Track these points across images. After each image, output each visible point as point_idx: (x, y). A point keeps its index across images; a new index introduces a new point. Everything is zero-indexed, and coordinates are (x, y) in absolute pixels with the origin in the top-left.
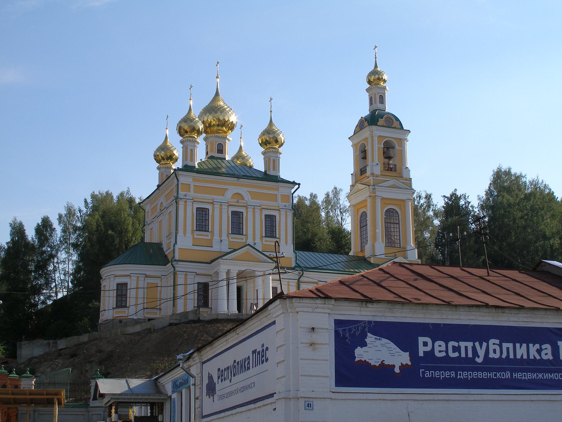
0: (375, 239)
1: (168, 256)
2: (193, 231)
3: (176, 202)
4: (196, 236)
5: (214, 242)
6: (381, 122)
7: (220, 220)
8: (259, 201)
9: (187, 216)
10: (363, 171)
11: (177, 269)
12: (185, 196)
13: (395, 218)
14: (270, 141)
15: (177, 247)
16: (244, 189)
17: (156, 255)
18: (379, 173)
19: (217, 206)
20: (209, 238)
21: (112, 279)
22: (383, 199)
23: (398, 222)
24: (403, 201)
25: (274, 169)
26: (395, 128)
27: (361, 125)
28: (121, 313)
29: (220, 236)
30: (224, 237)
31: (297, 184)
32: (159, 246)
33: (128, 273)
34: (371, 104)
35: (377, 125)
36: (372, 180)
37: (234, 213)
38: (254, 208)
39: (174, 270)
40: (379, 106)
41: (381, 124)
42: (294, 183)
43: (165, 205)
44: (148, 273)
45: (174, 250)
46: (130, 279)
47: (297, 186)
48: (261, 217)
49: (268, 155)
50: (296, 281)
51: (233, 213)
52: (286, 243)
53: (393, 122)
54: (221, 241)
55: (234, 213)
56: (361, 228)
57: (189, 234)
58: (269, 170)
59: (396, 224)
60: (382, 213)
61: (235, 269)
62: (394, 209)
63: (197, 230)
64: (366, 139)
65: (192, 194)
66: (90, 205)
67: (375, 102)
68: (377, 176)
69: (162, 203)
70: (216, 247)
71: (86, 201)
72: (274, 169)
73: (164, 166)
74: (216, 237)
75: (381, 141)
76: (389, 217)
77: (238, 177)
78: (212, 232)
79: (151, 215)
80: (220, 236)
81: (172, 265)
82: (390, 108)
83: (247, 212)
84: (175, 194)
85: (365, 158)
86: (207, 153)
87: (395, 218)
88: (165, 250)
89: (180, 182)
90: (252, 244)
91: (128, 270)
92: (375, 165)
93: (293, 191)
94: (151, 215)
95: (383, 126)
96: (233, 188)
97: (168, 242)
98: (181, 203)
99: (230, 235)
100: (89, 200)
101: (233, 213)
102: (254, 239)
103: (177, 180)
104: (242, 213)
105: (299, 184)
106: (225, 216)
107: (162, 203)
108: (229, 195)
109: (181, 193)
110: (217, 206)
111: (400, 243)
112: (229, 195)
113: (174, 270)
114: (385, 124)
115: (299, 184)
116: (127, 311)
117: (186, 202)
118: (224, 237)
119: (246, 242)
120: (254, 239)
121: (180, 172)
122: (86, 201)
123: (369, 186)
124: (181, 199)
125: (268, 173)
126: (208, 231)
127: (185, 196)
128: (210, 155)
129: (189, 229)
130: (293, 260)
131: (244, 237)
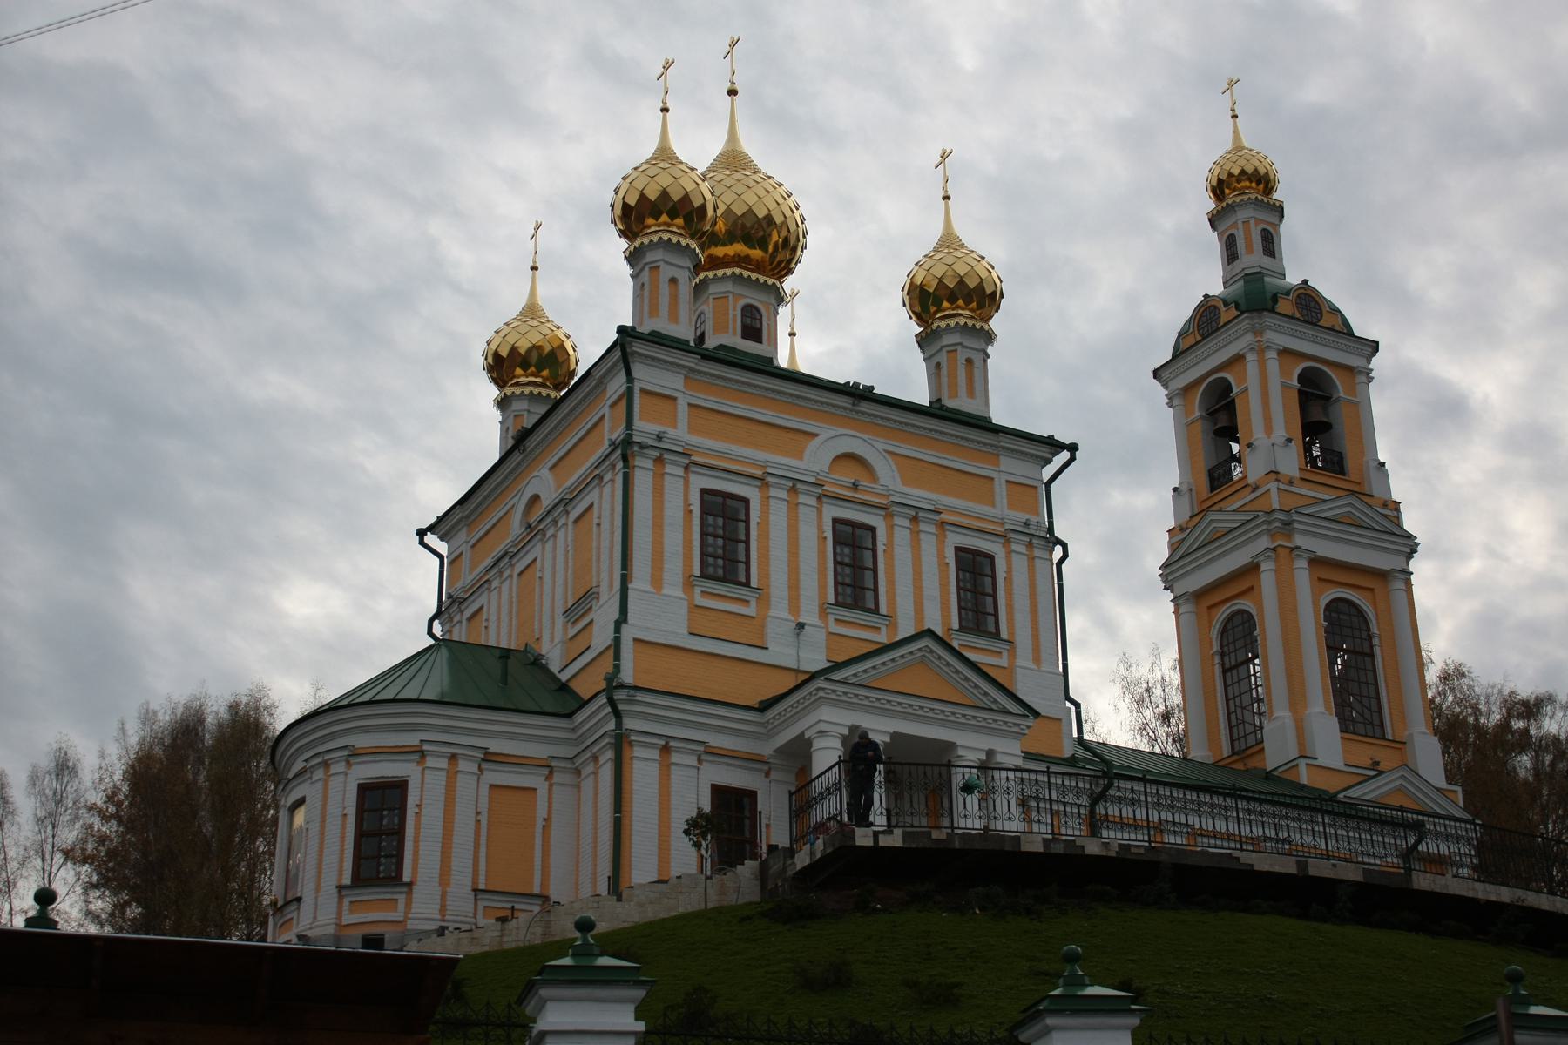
0: (1297, 698)
4: (700, 600)
5: (773, 629)
9: (669, 514)
10: (1218, 477)
11: (629, 723)
12: (659, 438)
13: (1357, 633)
14: (953, 305)
15: (628, 633)
18: (1296, 474)
21: (341, 767)
22: (1316, 562)
23: (1367, 650)
25: (971, 392)
28: (374, 914)
29: (794, 607)
30: (810, 615)
33: (412, 740)
36: (1274, 492)
39: (619, 725)
41: (1289, 313)
42: (1054, 445)
44: (495, 746)
45: (617, 642)
46: (549, 777)
47: (1065, 455)
48: (941, 555)
54: (801, 626)
56: (1224, 671)
57: (673, 588)
60: (1316, 611)
64: (1239, 358)
65: (681, 432)
67: (1250, 250)
68: (1291, 483)
69: (535, 499)
70: (781, 651)
72: (971, 392)
73: (527, 390)
74: (779, 609)
78: (762, 593)
79: (472, 569)
80: (794, 607)
83: (891, 528)
87: (1357, 633)
88: (554, 667)
89: (637, 386)
90: (939, 631)
91: (413, 728)
92: (1270, 444)
93: (1048, 471)
94: (472, 569)
97: (572, 632)
105: (1073, 448)
107: (535, 499)
113: (619, 725)
115: (1073, 448)
116: (402, 899)
121: (638, 347)
124: (642, 446)
129: (674, 568)
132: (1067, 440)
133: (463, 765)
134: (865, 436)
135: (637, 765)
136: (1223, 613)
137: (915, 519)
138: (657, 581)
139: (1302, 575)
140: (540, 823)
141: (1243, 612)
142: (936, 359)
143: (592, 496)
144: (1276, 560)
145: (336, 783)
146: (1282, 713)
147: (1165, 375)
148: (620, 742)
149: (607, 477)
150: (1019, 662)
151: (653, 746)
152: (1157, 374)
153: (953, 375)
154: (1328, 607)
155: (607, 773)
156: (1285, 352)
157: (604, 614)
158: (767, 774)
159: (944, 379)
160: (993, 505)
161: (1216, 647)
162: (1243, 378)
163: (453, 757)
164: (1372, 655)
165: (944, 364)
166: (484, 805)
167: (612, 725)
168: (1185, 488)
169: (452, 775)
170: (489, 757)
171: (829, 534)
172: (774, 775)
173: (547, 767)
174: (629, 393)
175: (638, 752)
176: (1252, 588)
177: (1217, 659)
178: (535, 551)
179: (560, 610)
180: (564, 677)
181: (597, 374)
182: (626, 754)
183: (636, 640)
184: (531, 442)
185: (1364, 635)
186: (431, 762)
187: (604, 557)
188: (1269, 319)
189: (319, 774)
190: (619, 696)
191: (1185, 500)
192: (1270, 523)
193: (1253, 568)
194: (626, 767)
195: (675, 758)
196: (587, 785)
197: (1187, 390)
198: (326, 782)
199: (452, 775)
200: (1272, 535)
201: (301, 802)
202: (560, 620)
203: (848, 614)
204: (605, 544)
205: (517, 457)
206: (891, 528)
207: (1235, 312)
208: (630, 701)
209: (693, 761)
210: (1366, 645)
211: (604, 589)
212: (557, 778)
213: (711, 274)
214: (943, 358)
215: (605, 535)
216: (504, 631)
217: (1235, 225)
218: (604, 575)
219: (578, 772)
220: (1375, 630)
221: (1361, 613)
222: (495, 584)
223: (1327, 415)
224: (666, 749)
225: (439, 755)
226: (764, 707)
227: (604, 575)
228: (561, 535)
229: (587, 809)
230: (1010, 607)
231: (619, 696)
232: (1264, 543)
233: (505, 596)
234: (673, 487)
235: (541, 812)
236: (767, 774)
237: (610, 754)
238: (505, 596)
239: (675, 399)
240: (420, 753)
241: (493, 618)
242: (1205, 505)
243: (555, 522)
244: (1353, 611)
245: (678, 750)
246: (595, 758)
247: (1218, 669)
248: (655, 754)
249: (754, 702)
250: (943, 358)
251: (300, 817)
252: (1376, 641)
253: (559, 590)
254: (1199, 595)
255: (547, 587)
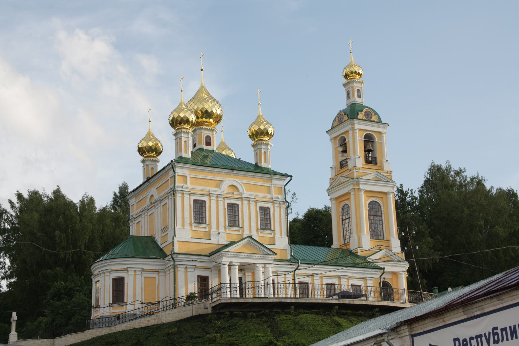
1: (163, 249)
2: (191, 224)
3: (174, 194)
6: (361, 116)
7: (216, 212)
8: (252, 193)
9: (184, 207)
10: (343, 164)
12: (182, 187)
13: (377, 210)
14: (258, 135)
16: (240, 180)
17: (150, 248)
19: (213, 198)
20: (207, 230)
22: (366, 191)
23: (380, 215)
24: (385, 193)
25: (265, 162)
26: (374, 121)
27: (339, 120)
29: (218, 228)
30: (222, 230)
31: (288, 176)
32: (151, 240)
33: (311, 272)
34: (349, 98)
35: (357, 119)
37: (230, 205)
38: (249, 200)
39: (174, 263)
40: (358, 100)
41: (361, 118)
42: (286, 175)
43: (156, 197)
44: (145, 267)
45: (173, 242)
46: (158, 274)
47: (289, 178)
48: (256, 209)
49: (147, 163)
50: (292, 273)
51: (230, 205)
52: (281, 235)
53: (371, 115)
54: (219, 233)
55: (230, 205)
56: (343, 220)
57: (187, 226)
58: (261, 162)
59: (379, 216)
60: (365, 204)
61: (237, 261)
62: (376, 202)
63: (195, 223)
64: (347, 132)
65: (189, 185)
66: (17, 205)
67: (354, 96)
68: (360, 169)
69: (152, 196)
70: (214, 240)
71: (11, 202)
74: (214, 230)
75: (357, 135)
76: (372, 210)
77: (233, 169)
78: (210, 224)
79: (137, 209)
80: (218, 228)
81: (172, 258)
82: (366, 101)
83: (242, 204)
84: (172, 186)
85: (345, 151)
86: (195, 146)
88: (159, 243)
89: (176, 174)
95: (362, 120)
96: (229, 180)
97: (163, 235)
98: (179, 196)
99: (259, 231)
100: (15, 200)
101: (230, 205)
102: (250, 231)
103: (174, 171)
104: (238, 205)
105: (291, 176)
106: (221, 208)
107: (152, 196)
108: (225, 188)
109: (178, 184)
110: (213, 198)
111: (383, 236)
112: (225, 188)
113: (174, 263)
114: (364, 118)
115: (291, 176)
117: (183, 194)
118: (222, 230)
119: (243, 234)
120: (250, 231)
121: (176, 164)
122: (11, 202)
123: (352, 179)
125: (259, 165)
126: (205, 223)
127: (182, 187)
128: (198, 147)
129: (187, 221)
130: (289, 251)
131: (240, 229)
132: (290, 175)
133: (137, 273)
134: (236, 180)
135: (179, 272)
136: (342, 204)
137: (249, 201)
138: (183, 225)
139: (363, 195)
140: (157, 286)
141: (347, 204)
142: (256, 152)
143: (166, 201)
144: (355, 192)
145: (107, 278)
146: (355, 235)
147: (329, 133)
148: (175, 267)
149: (170, 197)
150: (276, 236)
151: (183, 267)
152: (327, 132)
153: (261, 156)
154: (370, 204)
155: (172, 274)
156: (361, 130)
157: (170, 233)
158: (211, 272)
159: (258, 158)
160: (270, 194)
161: (341, 214)
162: (348, 136)
163: (135, 271)
164: (381, 216)
165: (258, 153)
166: (143, 282)
167: (172, 263)
168: (334, 167)
169: (135, 275)
170: (144, 270)
171: (226, 208)
172: (213, 272)
173: (157, 271)
174: (174, 176)
175: (179, 269)
176: (349, 199)
177: (341, 217)
178: (153, 210)
179: (160, 229)
180: (161, 247)
181: (167, 169)
182: (176, 269)
183: (178, 241)
184: (151, 181)
185: (380, 210)
186: (130, 272)
187: (170, 218)
188: (356, 121)
189: (103, 275)
190: (174, 256)
191: (334, 171)
192: (353, 181)
193: (348, 193)
194: (176, 272)
195: (188, 270)
196: (168, 276)
197: (335, 138)
198: (105, 277)
199: (135, 275)
200: (354, 185)
201: (99, 281)
202: (160, 232)
203: (231, 228)
204: (170, 215)
205: (147, 184)
206: (242, 204)
207: (347, 118)
208: (177, 257)
209: (193, 270)
210: (380, 213)
211: (170, 226)
212: (160, 274)
213: (197, 127)
214: (258, 151)
215: (170, 212)
216: (146, 233)
217: (349, 88)
218: (170, 223)
219: (165, 272)
220: (382, 209)
221: (379, 205)
222: (143, 216)
223: (373, 147)
224: (186, 268)
225: (132, 271)
226: (211, 255)
227: (170, 223)
228: (159, 208)
229: (168, 282)
230: (274, 221)
231: (174, 256)
232: (352, 187)
233: (146, 221)
234: (186, 200)
235: (157, 283)
236: (211, 272)
237: (172, 270)
238: (146, 221)
239: (186, 176)
240: (126, 270)
241: (143, 225)
242: (339, 172)
243: (158, 205)
244: (377, 204)
245: (189, 268)
246: (169, 270)
247: (341, 220)
248: (183, 269)
249: (207, 254)
250: (258, 151)
251: (98, 285)
252: (383, 212)
253: (159, 224)
254: (337, 199)
255: (156, 221)
